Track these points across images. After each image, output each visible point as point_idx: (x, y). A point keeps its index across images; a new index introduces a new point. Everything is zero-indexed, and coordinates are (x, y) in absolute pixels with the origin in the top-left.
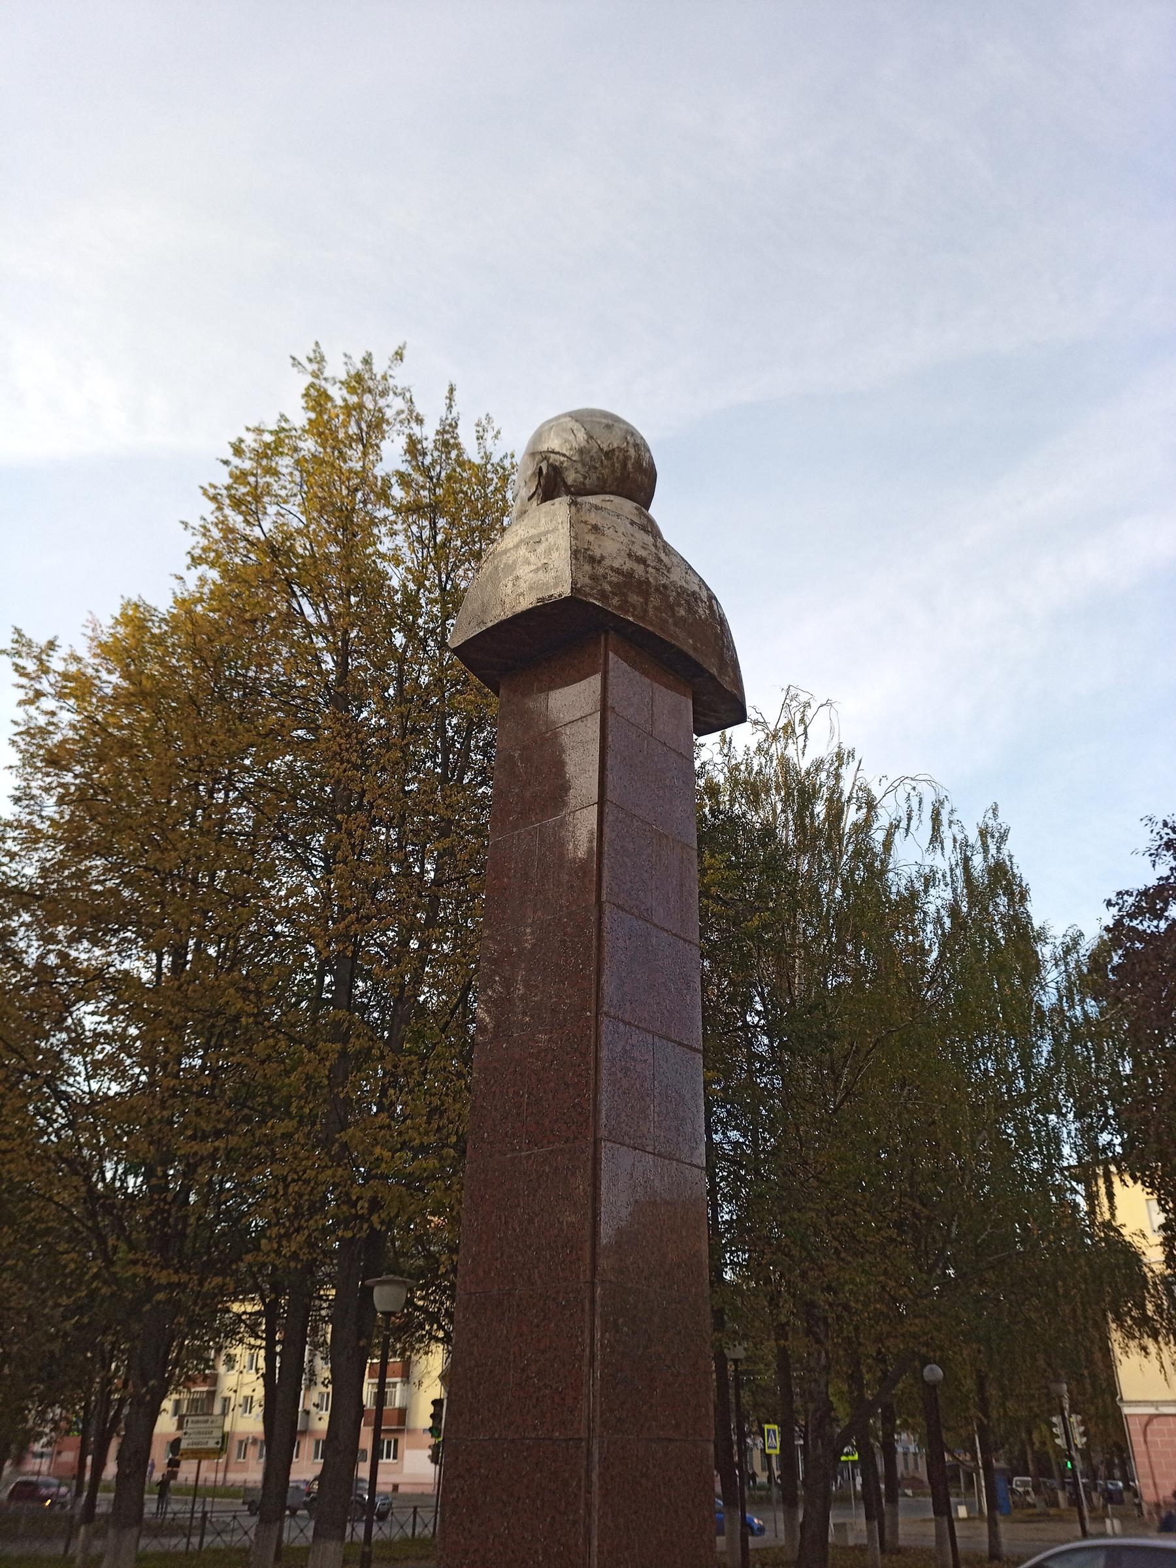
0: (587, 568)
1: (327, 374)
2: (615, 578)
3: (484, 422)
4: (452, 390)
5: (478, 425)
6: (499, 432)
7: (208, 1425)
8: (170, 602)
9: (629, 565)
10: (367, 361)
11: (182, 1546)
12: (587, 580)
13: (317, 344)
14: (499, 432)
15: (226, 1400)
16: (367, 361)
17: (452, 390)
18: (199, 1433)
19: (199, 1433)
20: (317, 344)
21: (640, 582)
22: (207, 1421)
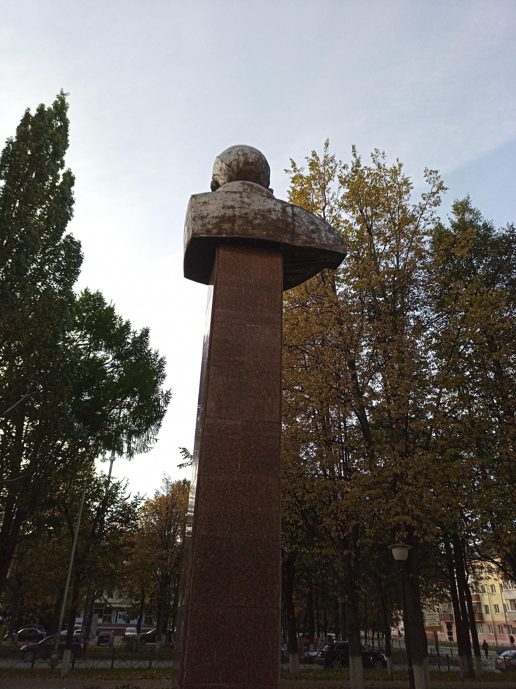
0: (200, 222)
1: (298, 168)
2: (215, 221)
3: (374, 153)
4: (353, 147)
5: (372, 156)
6: (383, 154)
7: (434, 616)
8: (95, 292)
9: (223, 212)
10: (314, 154)
11: (116, 663)
12: (200, 228)
13: (291, 159)
14: (383, 154)
15: (486, 606)
16: (314, 154)
17: (353, 147)
18: (432, 619)
19: (432, 619)
20: (291, 159)
21: (229, 217)
22: (433, 614)
